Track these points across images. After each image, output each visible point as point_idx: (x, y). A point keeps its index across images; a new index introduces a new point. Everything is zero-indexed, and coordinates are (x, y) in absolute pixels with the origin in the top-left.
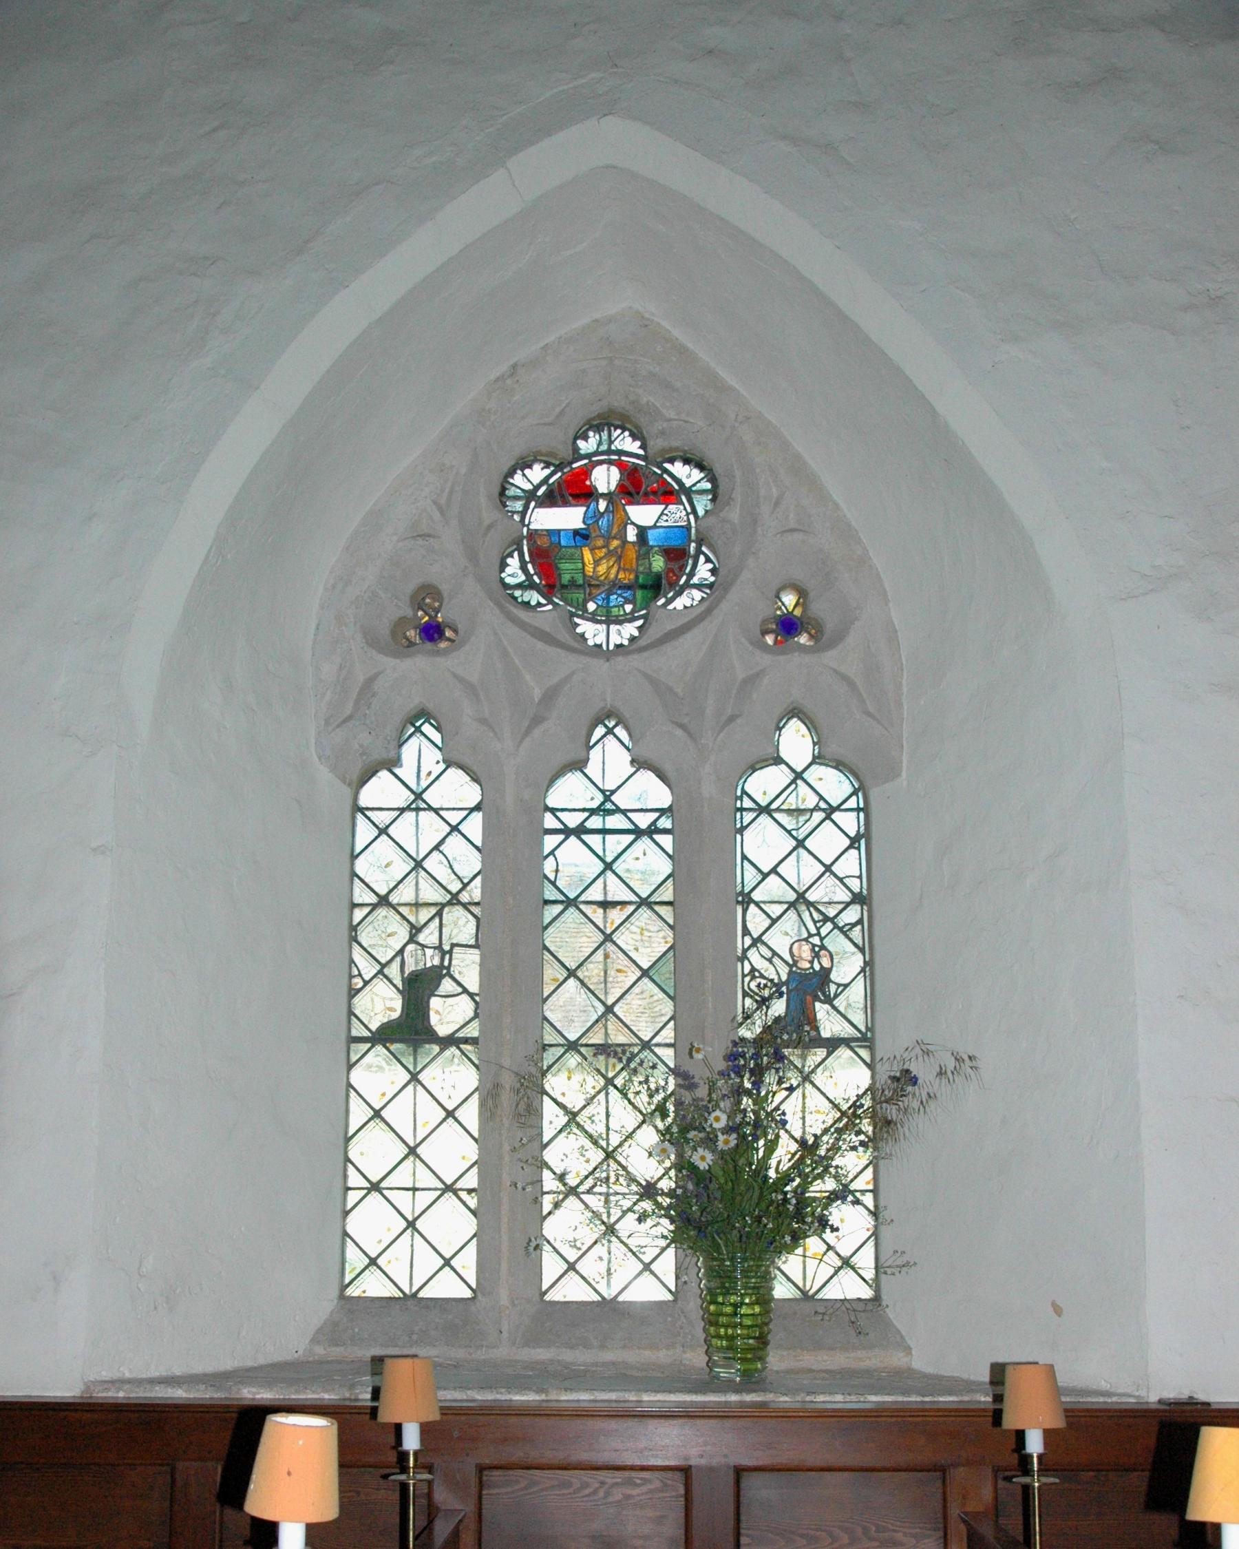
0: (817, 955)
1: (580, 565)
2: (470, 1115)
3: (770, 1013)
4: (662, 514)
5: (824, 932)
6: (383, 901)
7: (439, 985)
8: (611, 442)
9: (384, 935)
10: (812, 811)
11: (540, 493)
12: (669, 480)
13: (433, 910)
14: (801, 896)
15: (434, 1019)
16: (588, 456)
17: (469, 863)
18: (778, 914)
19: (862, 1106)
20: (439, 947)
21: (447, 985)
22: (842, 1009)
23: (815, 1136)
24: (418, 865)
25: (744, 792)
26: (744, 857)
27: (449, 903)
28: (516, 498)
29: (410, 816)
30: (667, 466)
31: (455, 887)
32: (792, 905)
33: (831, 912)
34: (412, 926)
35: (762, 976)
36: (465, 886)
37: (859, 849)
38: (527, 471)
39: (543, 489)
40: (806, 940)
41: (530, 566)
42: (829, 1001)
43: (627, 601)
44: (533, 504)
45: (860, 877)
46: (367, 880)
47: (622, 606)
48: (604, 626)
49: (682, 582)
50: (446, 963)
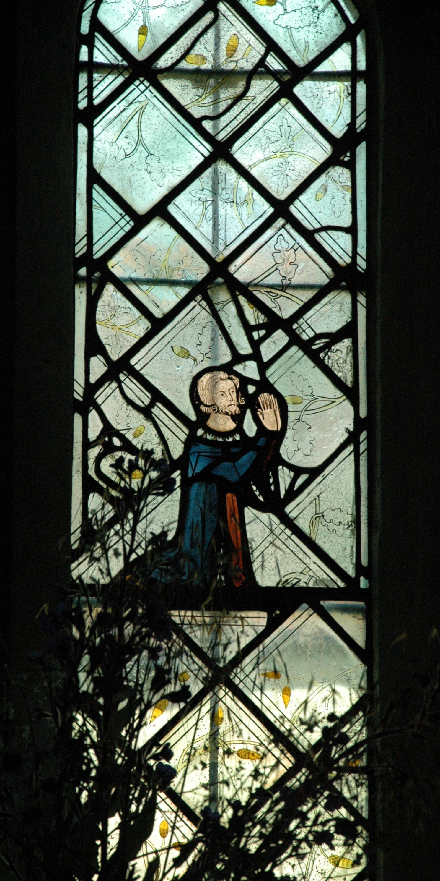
0: (250, 403)
3: (140, 527)
5: (267, 351)
10: (250, 75)
14: (220, 269)
18: (167, 308)
19: (345, 739)
22: (303, 524)
23: (236, 805)
25: (97, 26)
26: (94, 178)
32: (199, 290)
33: (286, 308)
35: (128, 446)
37: (351, 166)
40: (228, 368)
42: (275, 505)
45: (352, 230)
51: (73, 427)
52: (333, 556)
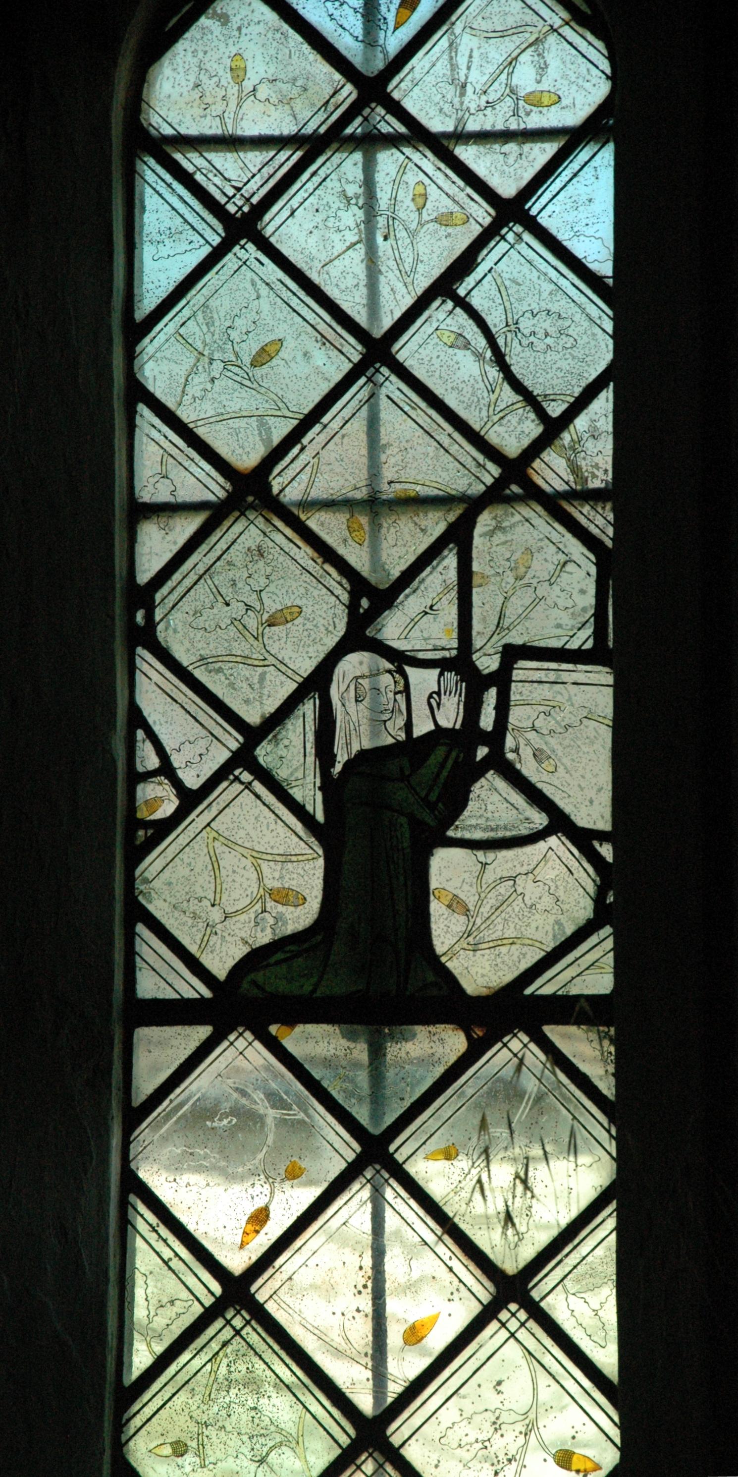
2: (588, 1303)
6: (250, 491)
7: (461, 803)
9: (238, 626)
13: (436, 524)
15: (445, 928)
17: (571, 340)
20: (460, 663)
21: (492, 804)
24: (377, 352)
27: (494, 495)
29: (348, 166)
31: (515, 432)
34: (358, 584)
36: (553, 429)
46: (186, 415)
50: (487, 720)
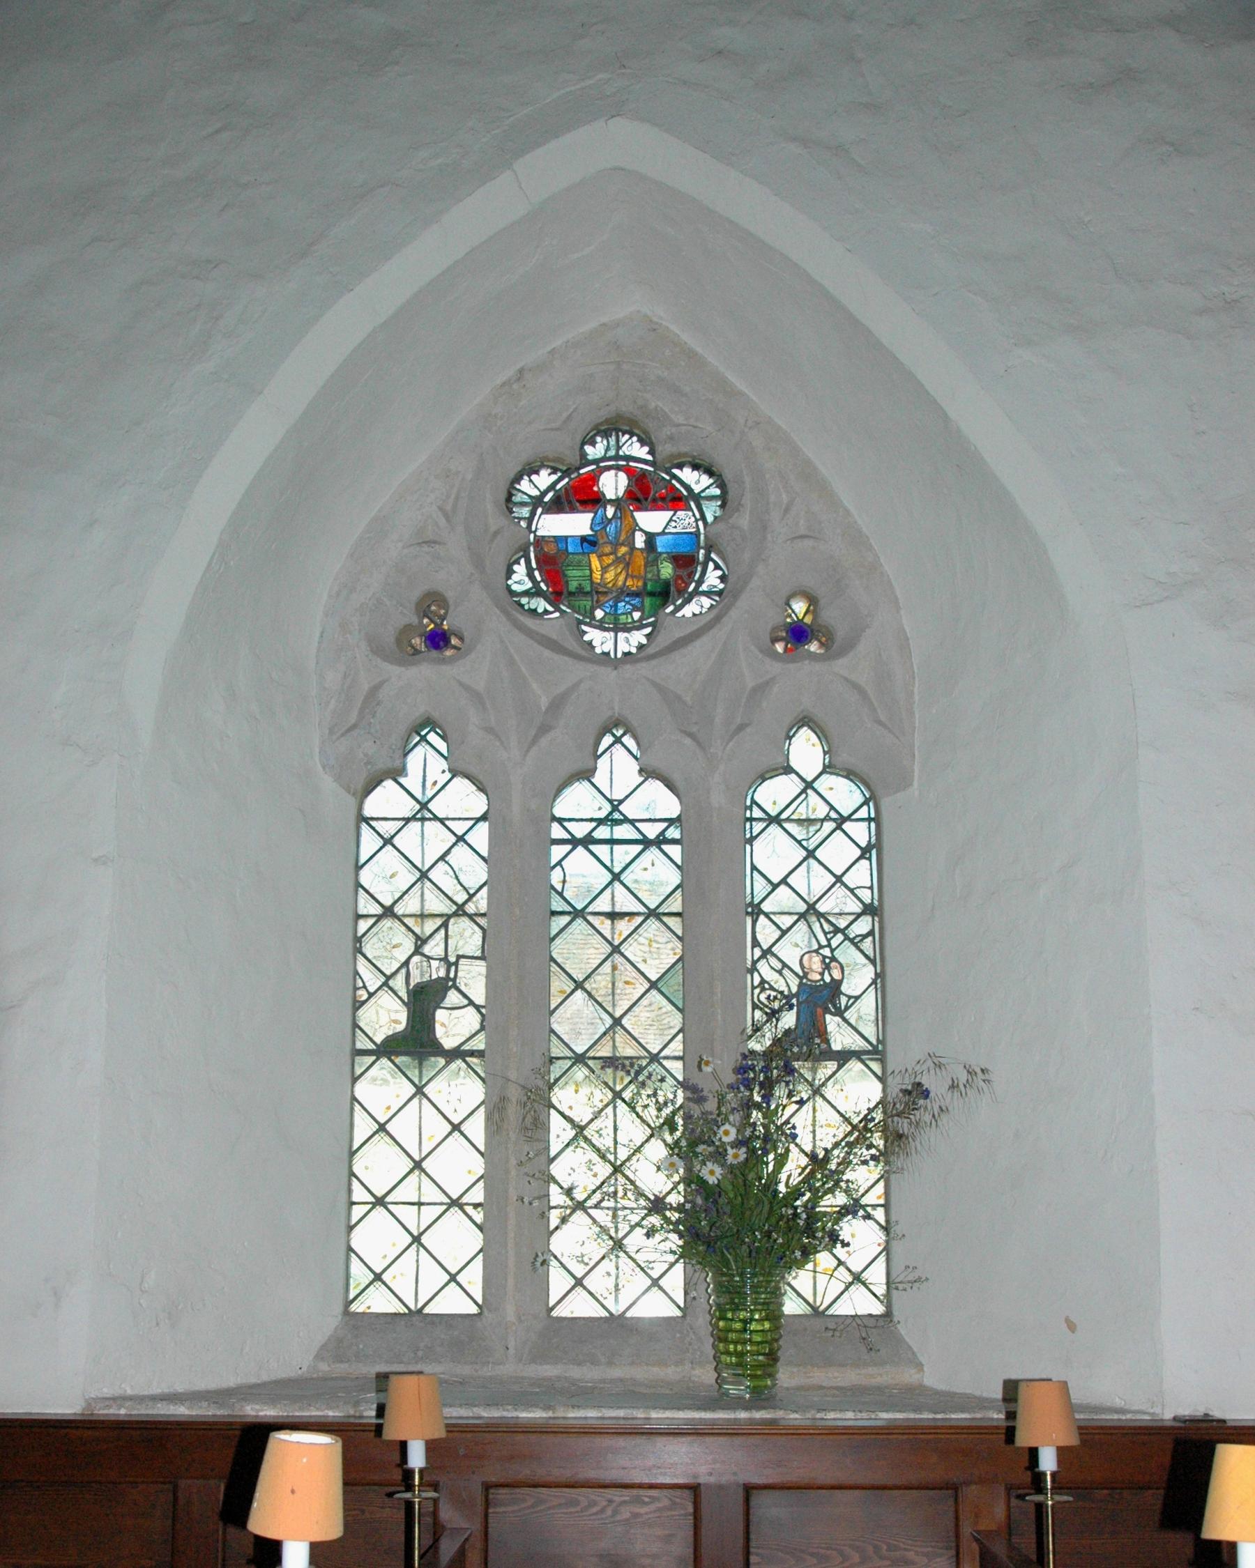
0: (827, 967)
1: (587, 572)
2: (477, 1128)
3: (779, 1025)
4: (671, 520)
5: (834, 943)
6: (388, 912)
7: (444, 997)
8: (619, 448)
10: (822, 821)
11: (547, 499)
12: (678, 485)
13: (439, 922)
14: (811, 907)
15: (439, 1032)
16: (596, 462)
17: (475, 873)
18: (788, 925)
19: (873, 1119)
20: (445, 959)
21: (453, 998)
22: (853, 1021)
23: (826, 1150)
24: (424, 875)
25: (753, 802)
26: (754, 868)
27: (455, 914)
28: (523, 504)
29: (415, 826)
30: (676, 471)
31: (461, 897)
32: (802, 916)
33: (842, 923)
34: (417, 937)
35: (772, 988)
36: (471, 896)
37: (870, 859)
38: (534, 477)
39: (550, 495)
40: (816, 951)
41: (537, 573)
42: (840, 1013)
43: (635, 609)
44: (539, 510)
45: (871, 888)
46: (371, 891)
47: (630, 613)
48: (612, 634)
49: (691, 589)
50: (452, 975)
51: (345, 1516)
52: (1034, 1536)
